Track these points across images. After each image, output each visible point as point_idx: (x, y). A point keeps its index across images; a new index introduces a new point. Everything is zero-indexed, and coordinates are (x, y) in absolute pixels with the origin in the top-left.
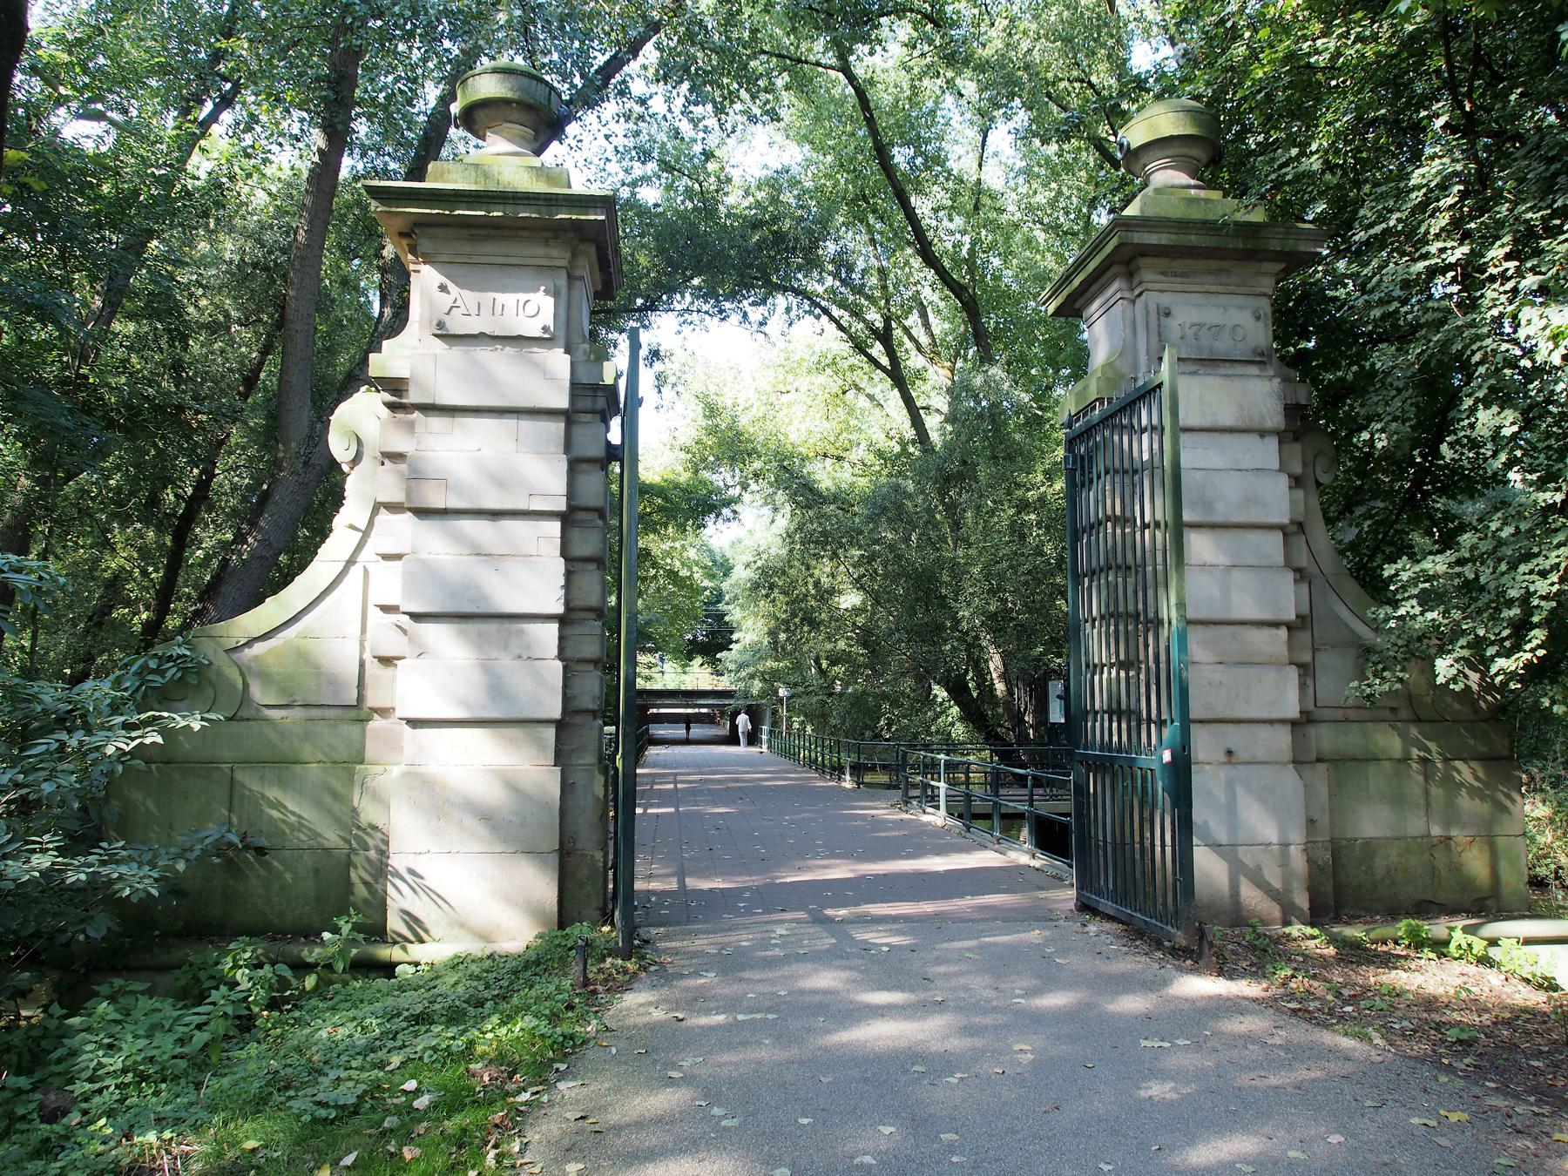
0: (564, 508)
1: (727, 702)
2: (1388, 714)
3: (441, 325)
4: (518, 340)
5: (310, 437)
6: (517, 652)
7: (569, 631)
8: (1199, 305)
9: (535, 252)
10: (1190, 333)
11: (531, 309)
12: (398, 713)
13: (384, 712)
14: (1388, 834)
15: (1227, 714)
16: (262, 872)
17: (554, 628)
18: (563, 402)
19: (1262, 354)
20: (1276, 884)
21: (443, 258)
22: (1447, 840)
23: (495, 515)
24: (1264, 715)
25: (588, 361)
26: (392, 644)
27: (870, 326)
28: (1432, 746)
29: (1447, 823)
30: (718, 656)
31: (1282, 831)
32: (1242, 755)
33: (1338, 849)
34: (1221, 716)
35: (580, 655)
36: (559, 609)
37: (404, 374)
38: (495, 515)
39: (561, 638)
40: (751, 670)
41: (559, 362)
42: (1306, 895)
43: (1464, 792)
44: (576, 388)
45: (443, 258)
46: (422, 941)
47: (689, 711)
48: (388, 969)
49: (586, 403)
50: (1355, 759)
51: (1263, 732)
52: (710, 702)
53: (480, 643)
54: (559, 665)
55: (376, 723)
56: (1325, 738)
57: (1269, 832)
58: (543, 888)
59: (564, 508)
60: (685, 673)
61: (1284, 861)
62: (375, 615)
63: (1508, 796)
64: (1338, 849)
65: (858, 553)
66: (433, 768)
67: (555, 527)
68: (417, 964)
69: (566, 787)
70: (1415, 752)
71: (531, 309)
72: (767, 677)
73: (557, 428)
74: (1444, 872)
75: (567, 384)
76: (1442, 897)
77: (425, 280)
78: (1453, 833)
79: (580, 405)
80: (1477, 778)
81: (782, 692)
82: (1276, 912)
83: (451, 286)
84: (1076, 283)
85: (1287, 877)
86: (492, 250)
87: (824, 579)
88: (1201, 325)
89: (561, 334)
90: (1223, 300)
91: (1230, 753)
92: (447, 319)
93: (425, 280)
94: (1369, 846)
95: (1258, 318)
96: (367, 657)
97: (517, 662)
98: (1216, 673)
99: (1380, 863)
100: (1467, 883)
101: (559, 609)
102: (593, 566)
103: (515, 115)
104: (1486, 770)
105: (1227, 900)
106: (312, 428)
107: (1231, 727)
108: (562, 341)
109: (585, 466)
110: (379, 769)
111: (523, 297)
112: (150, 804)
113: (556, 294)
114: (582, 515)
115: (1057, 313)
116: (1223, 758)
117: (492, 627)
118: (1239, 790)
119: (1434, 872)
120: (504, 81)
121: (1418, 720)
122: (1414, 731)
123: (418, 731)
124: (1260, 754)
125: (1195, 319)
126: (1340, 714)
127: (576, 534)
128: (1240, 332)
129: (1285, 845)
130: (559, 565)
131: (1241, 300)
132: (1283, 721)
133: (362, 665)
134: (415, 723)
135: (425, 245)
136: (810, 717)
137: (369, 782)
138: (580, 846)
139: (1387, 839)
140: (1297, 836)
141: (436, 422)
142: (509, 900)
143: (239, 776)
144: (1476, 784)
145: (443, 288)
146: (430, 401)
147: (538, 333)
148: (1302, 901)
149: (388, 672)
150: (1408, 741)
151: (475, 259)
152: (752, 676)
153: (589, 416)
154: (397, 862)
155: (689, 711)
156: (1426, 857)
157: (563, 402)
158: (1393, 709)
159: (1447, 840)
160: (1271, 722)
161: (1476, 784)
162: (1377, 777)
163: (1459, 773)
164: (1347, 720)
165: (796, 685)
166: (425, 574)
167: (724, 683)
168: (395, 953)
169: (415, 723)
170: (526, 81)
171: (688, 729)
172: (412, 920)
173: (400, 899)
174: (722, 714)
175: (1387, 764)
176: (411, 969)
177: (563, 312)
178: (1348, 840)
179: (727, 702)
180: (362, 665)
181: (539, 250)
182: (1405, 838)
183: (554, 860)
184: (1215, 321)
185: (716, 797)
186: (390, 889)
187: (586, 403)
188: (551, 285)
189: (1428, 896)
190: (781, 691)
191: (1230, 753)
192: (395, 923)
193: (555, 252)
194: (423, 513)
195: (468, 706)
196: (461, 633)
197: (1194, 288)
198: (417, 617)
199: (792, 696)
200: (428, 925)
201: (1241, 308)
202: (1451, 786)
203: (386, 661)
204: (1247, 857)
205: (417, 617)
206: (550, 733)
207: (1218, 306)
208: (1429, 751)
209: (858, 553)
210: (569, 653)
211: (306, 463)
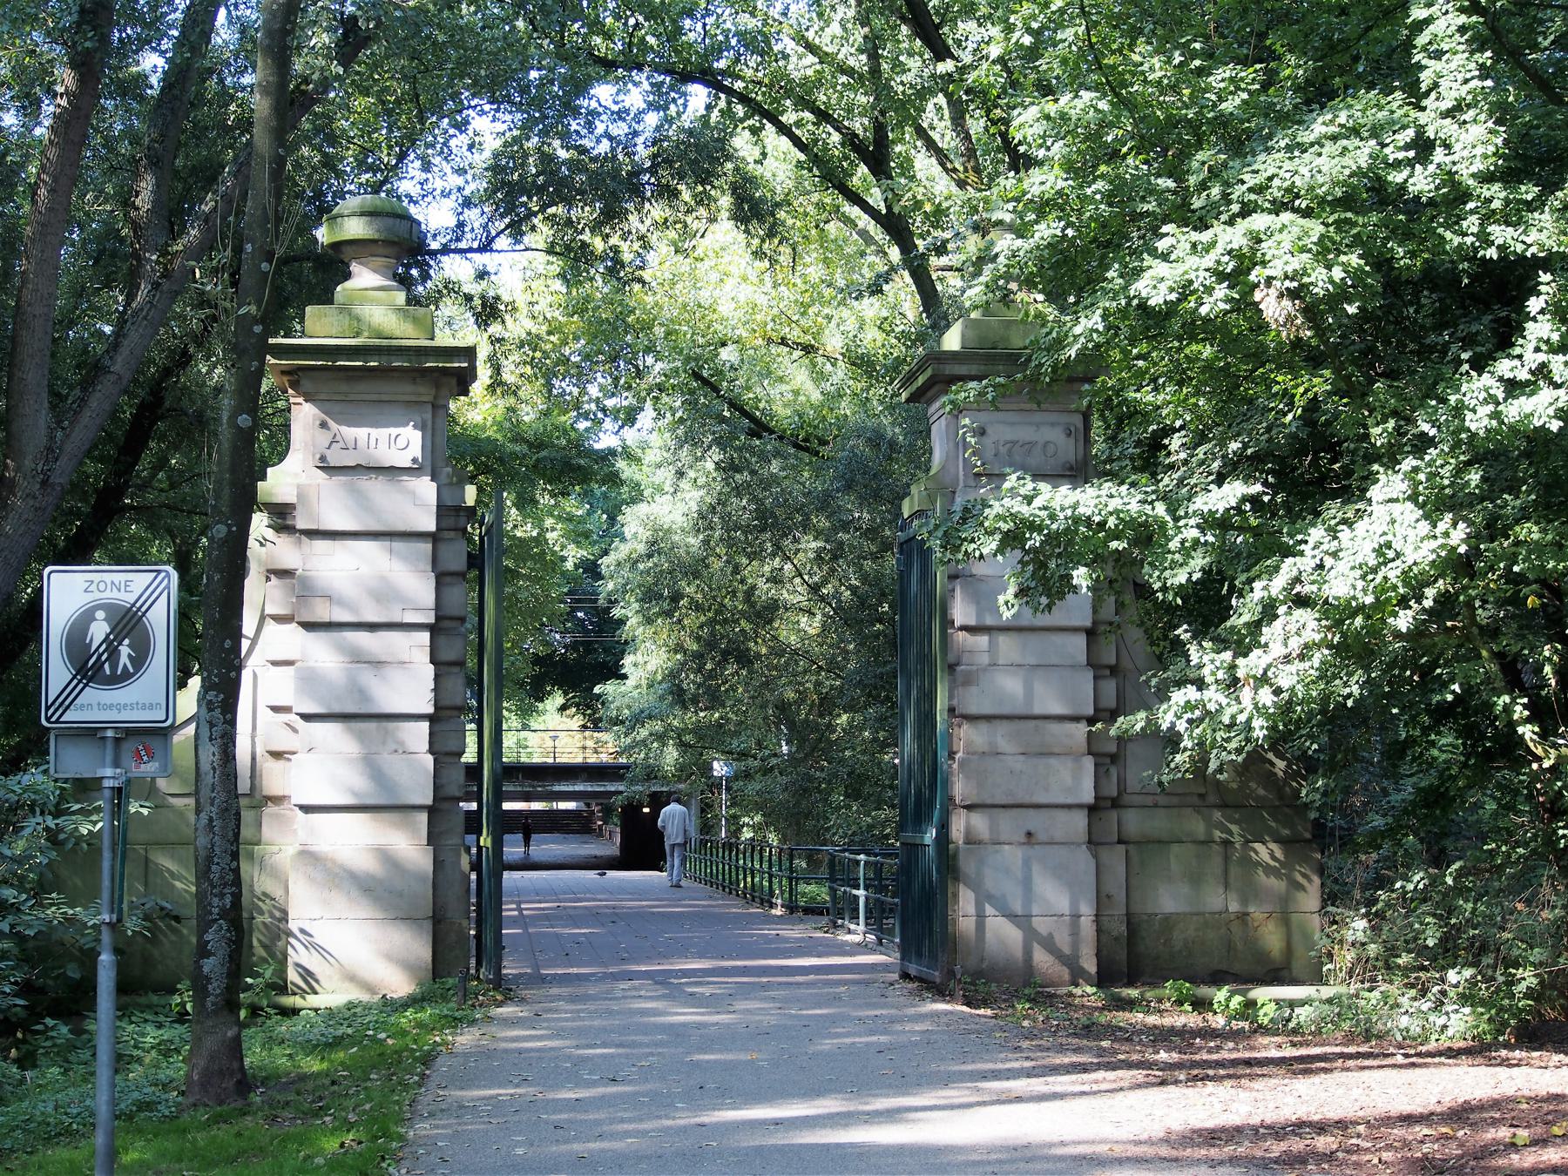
0: (432, 620)
1: (611, 788)
2: (1195, 800)
3: (323, 458)
4: (392, 471)
5: (50, 449)
6: (394, 747)
7: (437, 727)
8: (1013, 424)
9: (405, 390)
10: (1003, 450)
11: (401, 443)
12: (294, 801)
13: (278, 800)
14: (1188, 910)
15: (1027, 800)
16: (173, 938)
17: (425, 725)
18: (430, 525)
19: (1071, 469)
20: (1067, 950)
21: (322, 397)
22: (1243, 917)
23: (372, 627)
24: (1061, 800)
25: (451, 484)
26: (283, 741)
27: (850, 139)
28: (1234, 828)
29: (1244, 901)
30: (597, 690)
31: (1074, 903)
32: (1042, 837)
33: (1133, 923)
34: (1020, 801)
35: (448, 749)
36: (430, 710)
37: (291, 499)
38: (372, 627)
39: (431, 734)
40: (658, 726)
41: (426, 489)
42: (1095, 960)
43: (1260, 871)
44: (443, 510)
45: (322, 397)
46: (316, 993)
47: (537, 806)
48: (295, 1011)
49: (450, 522)
50: (1159, 842)
51: (1061, 815)
52: (579, 787)
53: (361, 738)
54: (430, 759)
55: (270, 809)
56: (1134, 822)
57: (1062, 903)
58: (421, 950)
59: (432, 620)
60: (525, 727)
61: (1075, 932)
62: (265, 715)
63: (1304, 876)
64: (1133, 923)
65: (814, 545)
66: (322, 846)
67: (425, 637)
68: (316, 1010)
69: (438, 863)
70: (1217, 834)
71: (401, 443)
72: (688, 738)
73: (427, 547)
74: (1240, 946)
75: (434, 509)
76: (1237, 967)
77: (304, 416)
78: (1251, 910)
79: (444, 525)
80: (1273, 857)
81: (719, 769)
82: (1065, 974)
83: (331, 423)
84: (921, 380)
85: (1075, 945)
86: (365, 389)
87: (762, 585)
88: (1014, 443)
89: (428, 463)
90: (1038, 417)
91: (1029, 834)
92: (328, 453)
93: (304, 416)
94: (1168, 921)
95: (1069, 435)
96: (259, 751)
97: (395, 756)
98: (1018, 763)
99: (1178, 937)
100: (1261, 956)
101: (430, 710)
102: (456, 669)
103: (381, 250)
104: (1286, 854)
105: (1021, 964)
106: (52, 438)
107: (1031, 812)
108: (429, 470)
109: (448, 579)
110: (275, 849)
111: (394, 431)
112: (79, 882)
113: (422, 427)
114: (447, 624)
115: (908, 401)
116: (1023, 839)
117: (371, 726)
118: (1036, 868)
119: (1229, 946)
120: (371, 223)
121: (1223, 806)
122: (1217, 815)
123: (310, 816)
124: (1059, 835)
125: (1009, 437)
126: (1149, 800)
127: (442, 640)
128: (1051, 449)
129: (1076, 917)
130: (429, 670)
131: (1053, 417)
132: (1080, 806)
133: (254, 759)
134: (307, 809)
135: (307, 384)
136: (773, 816)
137: (268, 860)
138: (449, 915)
139: (1185, 914)
140: (1087, 910)
141: (321, 545)
142: (389, 957)
143: (152, 857)
144: (1272, 863)
145: (323, 425)
146: (314, 527)
147: (409, 464)
148: (1091, 966)
149: (281, 764)
150: (1211, 825)
151: (352, 397)
152: (661, 738)
153: (452, 534)
154: (293, 926)
155: (537, 806)
156: (1223, 931)
157: (430, 525)
158: (1201, 796)
159: (1243, 917)
160: (1069, 807)
161: (1272, 863)
162: (1178, 856)
163: (1256, 853)
164: (1156, 806)
165: (743, 755)
166: (309, 680)
167: (604, 748)
168: (296, 1001)
169: (307, 809)
170: (390, 221)
171: (527, 843)
172: (307, 974)
173: (298, 955)
174: (607, 811)
175: (1215, 847)
176: (312, 1014)
177: (429, 444)
178: (1150, 915)
179: (611, 788)
180: (254, 759)
181: (409, 388)
182: (1203, 914)
183: (428, 925)
184: (1028, 439)
185: (575, 919)
186: (290, 950)
187: (450, 522)
188: (419, 420)
189: (1224, 967)
190: (716, 765)
191: (1029, 834)
192: (293, 976)
193: (422, 389)
194: (309, 626)
195: (355, 794)
196: (351, 730)
197: (1014, 407)
198: (307, 717)
199: (736, 777)
200: (319, 977)
201: (1053, 425)
202: (1250, 864)
203: (277, 755)
204: (1042, 925)
205: (307, 717)
206: (423, 817)
207: (1030, 424)
208: (1231, 833)
209: (814, 545)
210: (437, 748)
211: (44, 483)
